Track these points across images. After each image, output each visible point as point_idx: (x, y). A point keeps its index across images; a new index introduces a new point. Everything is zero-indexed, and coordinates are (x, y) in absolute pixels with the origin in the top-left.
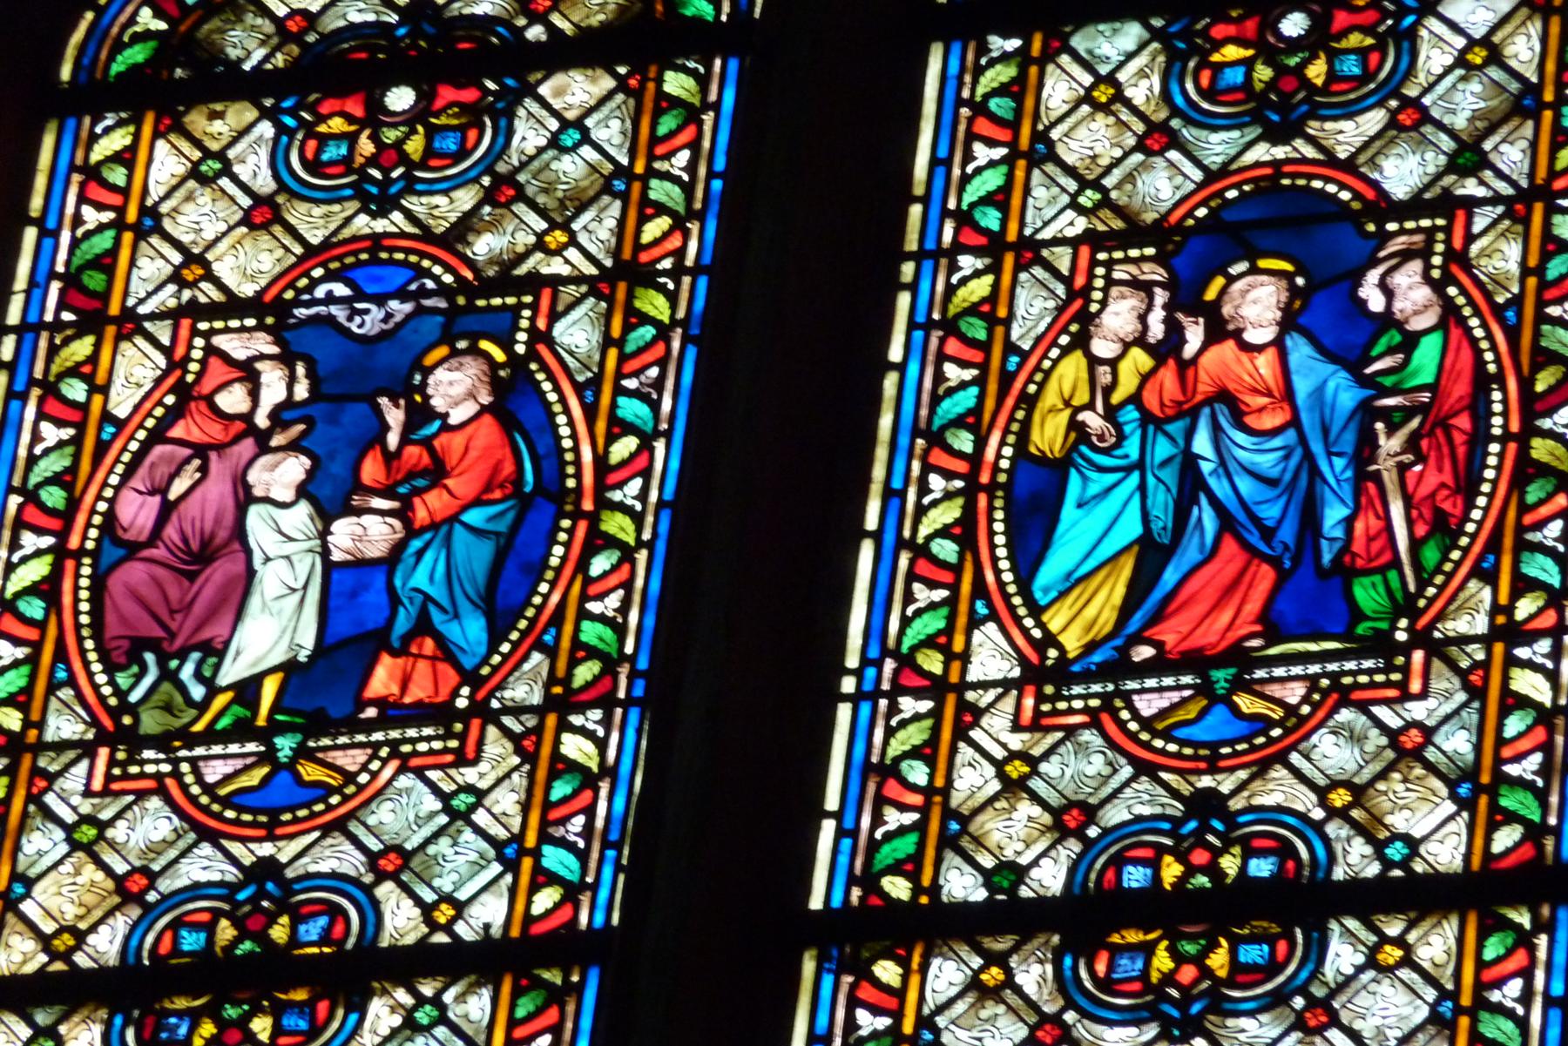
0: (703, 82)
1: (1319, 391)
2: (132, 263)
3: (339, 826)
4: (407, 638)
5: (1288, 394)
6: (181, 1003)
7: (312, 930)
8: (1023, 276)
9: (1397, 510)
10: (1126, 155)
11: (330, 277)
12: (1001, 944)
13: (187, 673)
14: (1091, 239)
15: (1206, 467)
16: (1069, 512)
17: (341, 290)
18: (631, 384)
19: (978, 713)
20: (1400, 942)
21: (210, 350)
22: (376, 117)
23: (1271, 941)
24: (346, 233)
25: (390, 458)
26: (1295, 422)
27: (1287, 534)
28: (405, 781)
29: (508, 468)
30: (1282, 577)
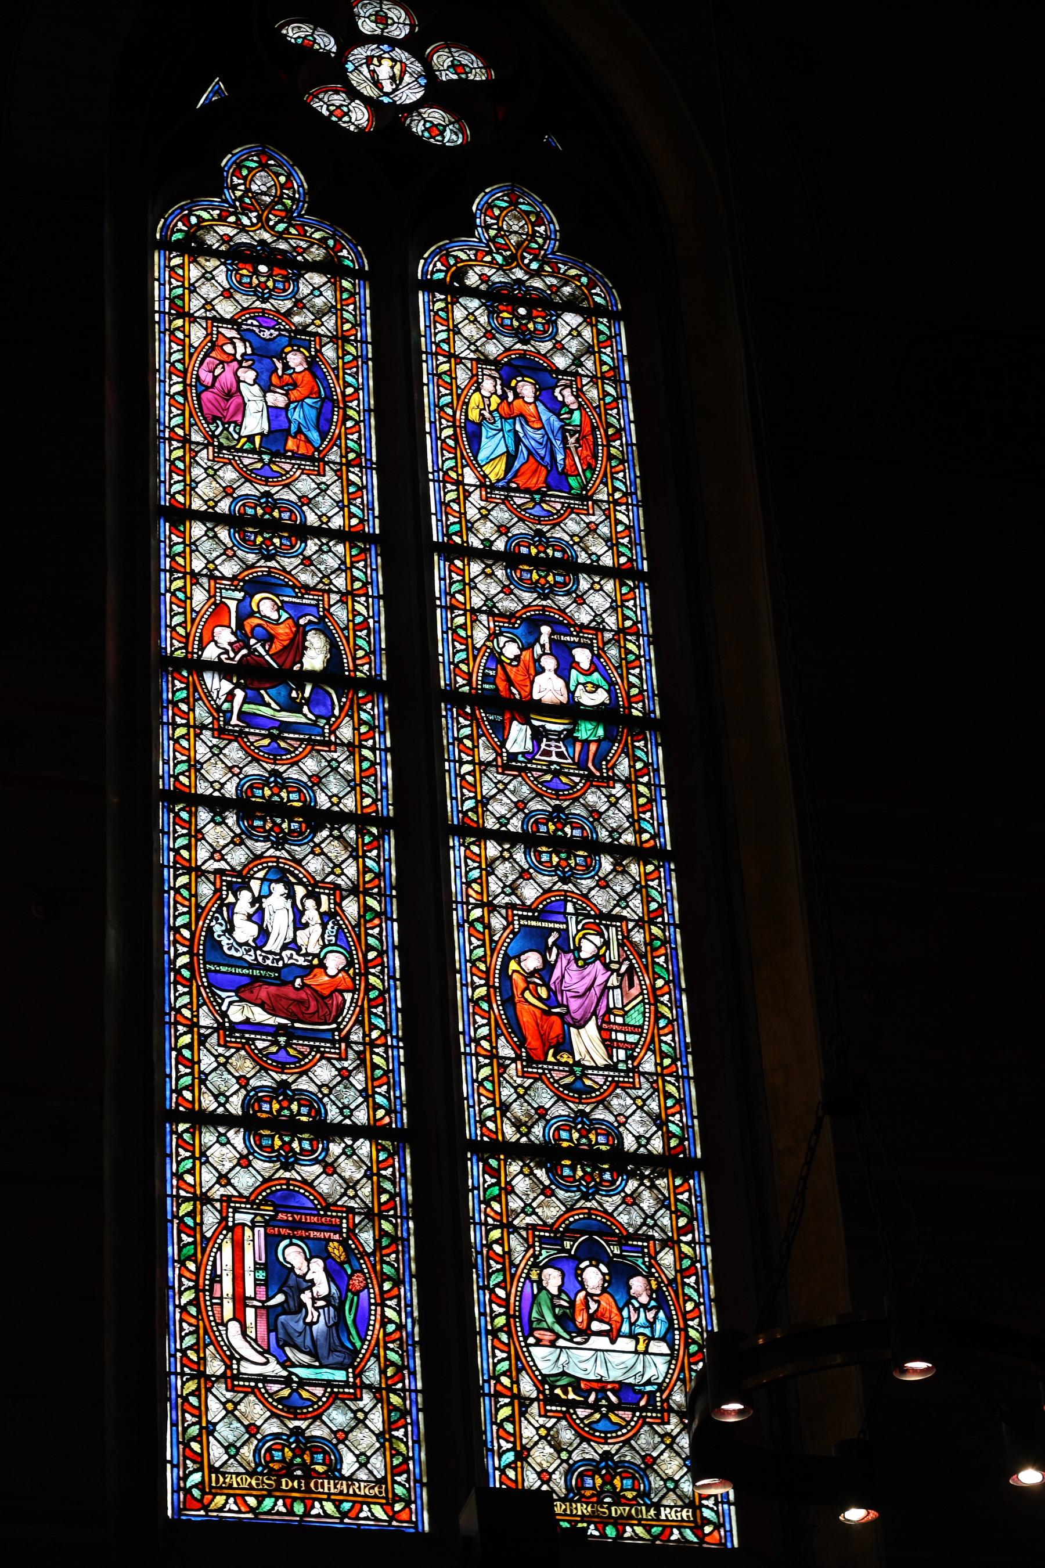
0: (354, 285)
1: (549, 419)
2: (190, 300)
3: (287, 486)
4: (296, 433)
5: (540, 419)
6: (251, 530)
7: (286, 515)
8: (204, 1208)
9: (577, 459)
10: (538, 1195)
11: (251, 318)
12: (490, 562)
13: (231, 429)
14: (478, 360)
15: (521, 435)
16: (484, 439)
17: (255, 323)
18: (348, 371)
19: (470, 493)
20: (599, 583)
21: (219, 333)
22: (256, 273)
23: (564, 576)
24: (253, 306)
25: (280, 378)
26: (543, 427)
27: (547, 459)
28: (304, 477)
29: (316, 389)
30: (548, 472)
